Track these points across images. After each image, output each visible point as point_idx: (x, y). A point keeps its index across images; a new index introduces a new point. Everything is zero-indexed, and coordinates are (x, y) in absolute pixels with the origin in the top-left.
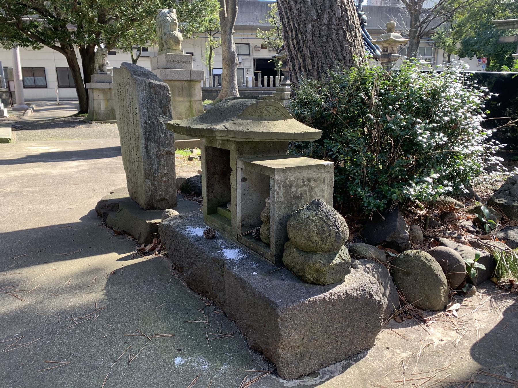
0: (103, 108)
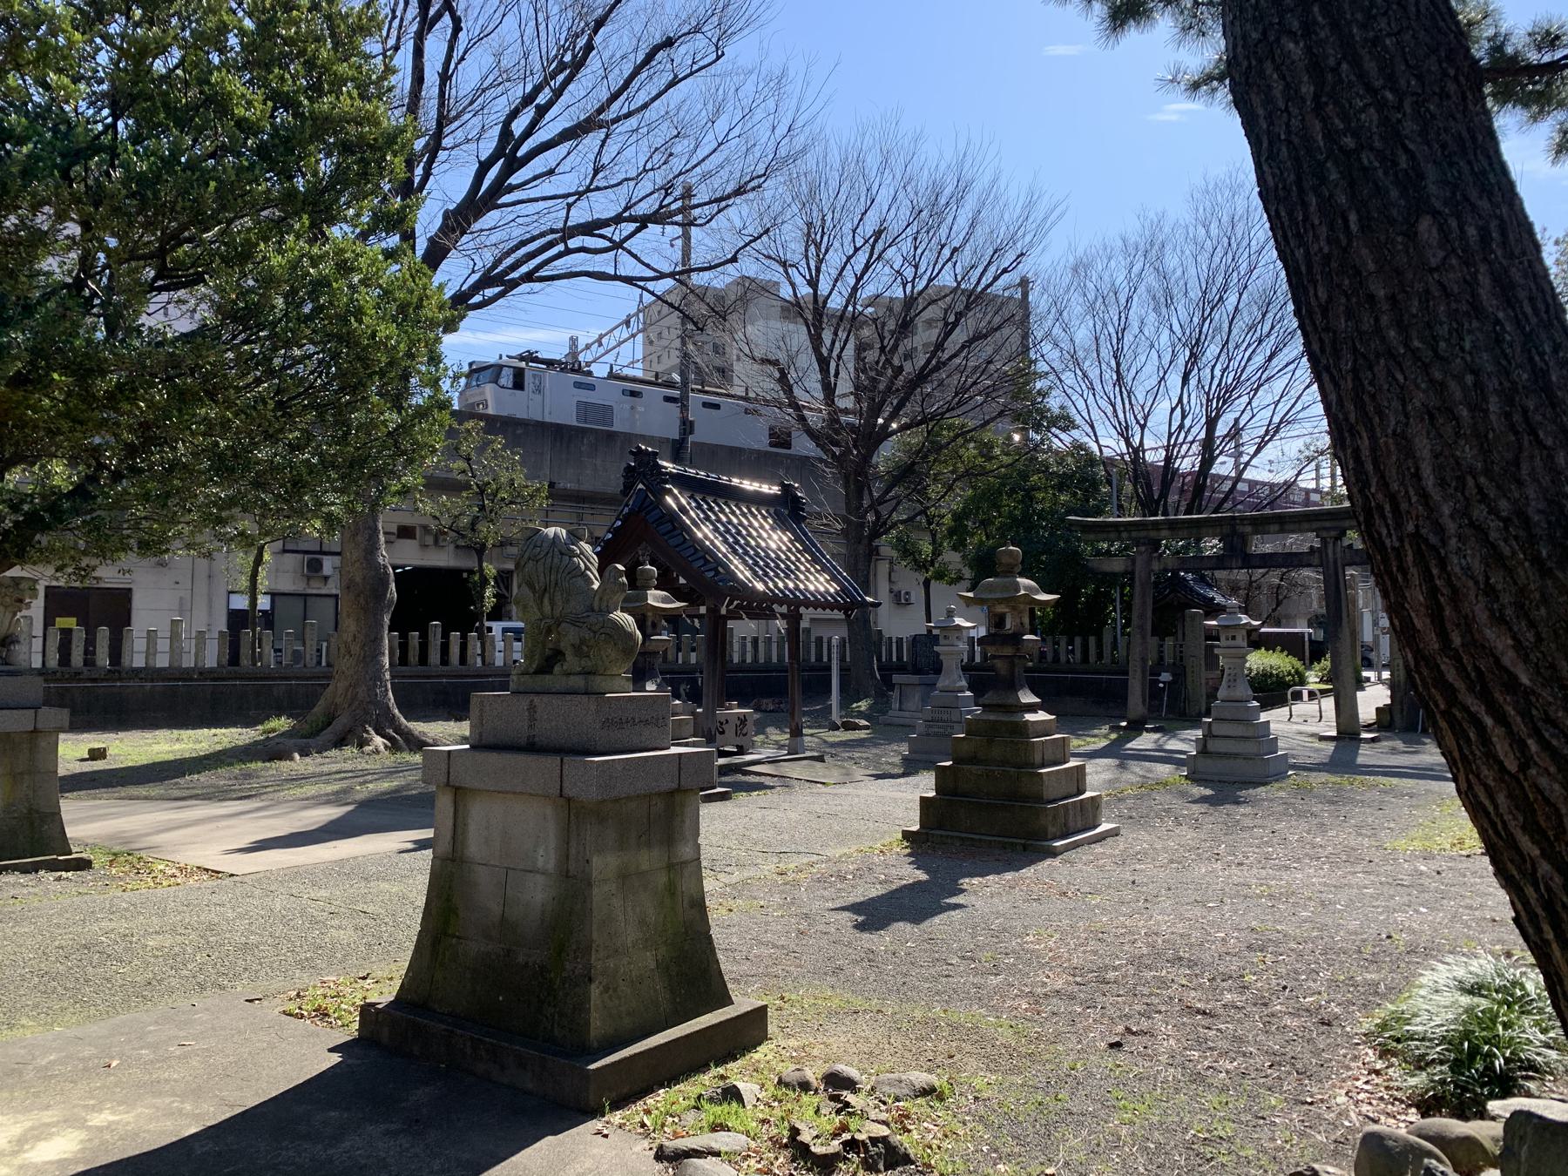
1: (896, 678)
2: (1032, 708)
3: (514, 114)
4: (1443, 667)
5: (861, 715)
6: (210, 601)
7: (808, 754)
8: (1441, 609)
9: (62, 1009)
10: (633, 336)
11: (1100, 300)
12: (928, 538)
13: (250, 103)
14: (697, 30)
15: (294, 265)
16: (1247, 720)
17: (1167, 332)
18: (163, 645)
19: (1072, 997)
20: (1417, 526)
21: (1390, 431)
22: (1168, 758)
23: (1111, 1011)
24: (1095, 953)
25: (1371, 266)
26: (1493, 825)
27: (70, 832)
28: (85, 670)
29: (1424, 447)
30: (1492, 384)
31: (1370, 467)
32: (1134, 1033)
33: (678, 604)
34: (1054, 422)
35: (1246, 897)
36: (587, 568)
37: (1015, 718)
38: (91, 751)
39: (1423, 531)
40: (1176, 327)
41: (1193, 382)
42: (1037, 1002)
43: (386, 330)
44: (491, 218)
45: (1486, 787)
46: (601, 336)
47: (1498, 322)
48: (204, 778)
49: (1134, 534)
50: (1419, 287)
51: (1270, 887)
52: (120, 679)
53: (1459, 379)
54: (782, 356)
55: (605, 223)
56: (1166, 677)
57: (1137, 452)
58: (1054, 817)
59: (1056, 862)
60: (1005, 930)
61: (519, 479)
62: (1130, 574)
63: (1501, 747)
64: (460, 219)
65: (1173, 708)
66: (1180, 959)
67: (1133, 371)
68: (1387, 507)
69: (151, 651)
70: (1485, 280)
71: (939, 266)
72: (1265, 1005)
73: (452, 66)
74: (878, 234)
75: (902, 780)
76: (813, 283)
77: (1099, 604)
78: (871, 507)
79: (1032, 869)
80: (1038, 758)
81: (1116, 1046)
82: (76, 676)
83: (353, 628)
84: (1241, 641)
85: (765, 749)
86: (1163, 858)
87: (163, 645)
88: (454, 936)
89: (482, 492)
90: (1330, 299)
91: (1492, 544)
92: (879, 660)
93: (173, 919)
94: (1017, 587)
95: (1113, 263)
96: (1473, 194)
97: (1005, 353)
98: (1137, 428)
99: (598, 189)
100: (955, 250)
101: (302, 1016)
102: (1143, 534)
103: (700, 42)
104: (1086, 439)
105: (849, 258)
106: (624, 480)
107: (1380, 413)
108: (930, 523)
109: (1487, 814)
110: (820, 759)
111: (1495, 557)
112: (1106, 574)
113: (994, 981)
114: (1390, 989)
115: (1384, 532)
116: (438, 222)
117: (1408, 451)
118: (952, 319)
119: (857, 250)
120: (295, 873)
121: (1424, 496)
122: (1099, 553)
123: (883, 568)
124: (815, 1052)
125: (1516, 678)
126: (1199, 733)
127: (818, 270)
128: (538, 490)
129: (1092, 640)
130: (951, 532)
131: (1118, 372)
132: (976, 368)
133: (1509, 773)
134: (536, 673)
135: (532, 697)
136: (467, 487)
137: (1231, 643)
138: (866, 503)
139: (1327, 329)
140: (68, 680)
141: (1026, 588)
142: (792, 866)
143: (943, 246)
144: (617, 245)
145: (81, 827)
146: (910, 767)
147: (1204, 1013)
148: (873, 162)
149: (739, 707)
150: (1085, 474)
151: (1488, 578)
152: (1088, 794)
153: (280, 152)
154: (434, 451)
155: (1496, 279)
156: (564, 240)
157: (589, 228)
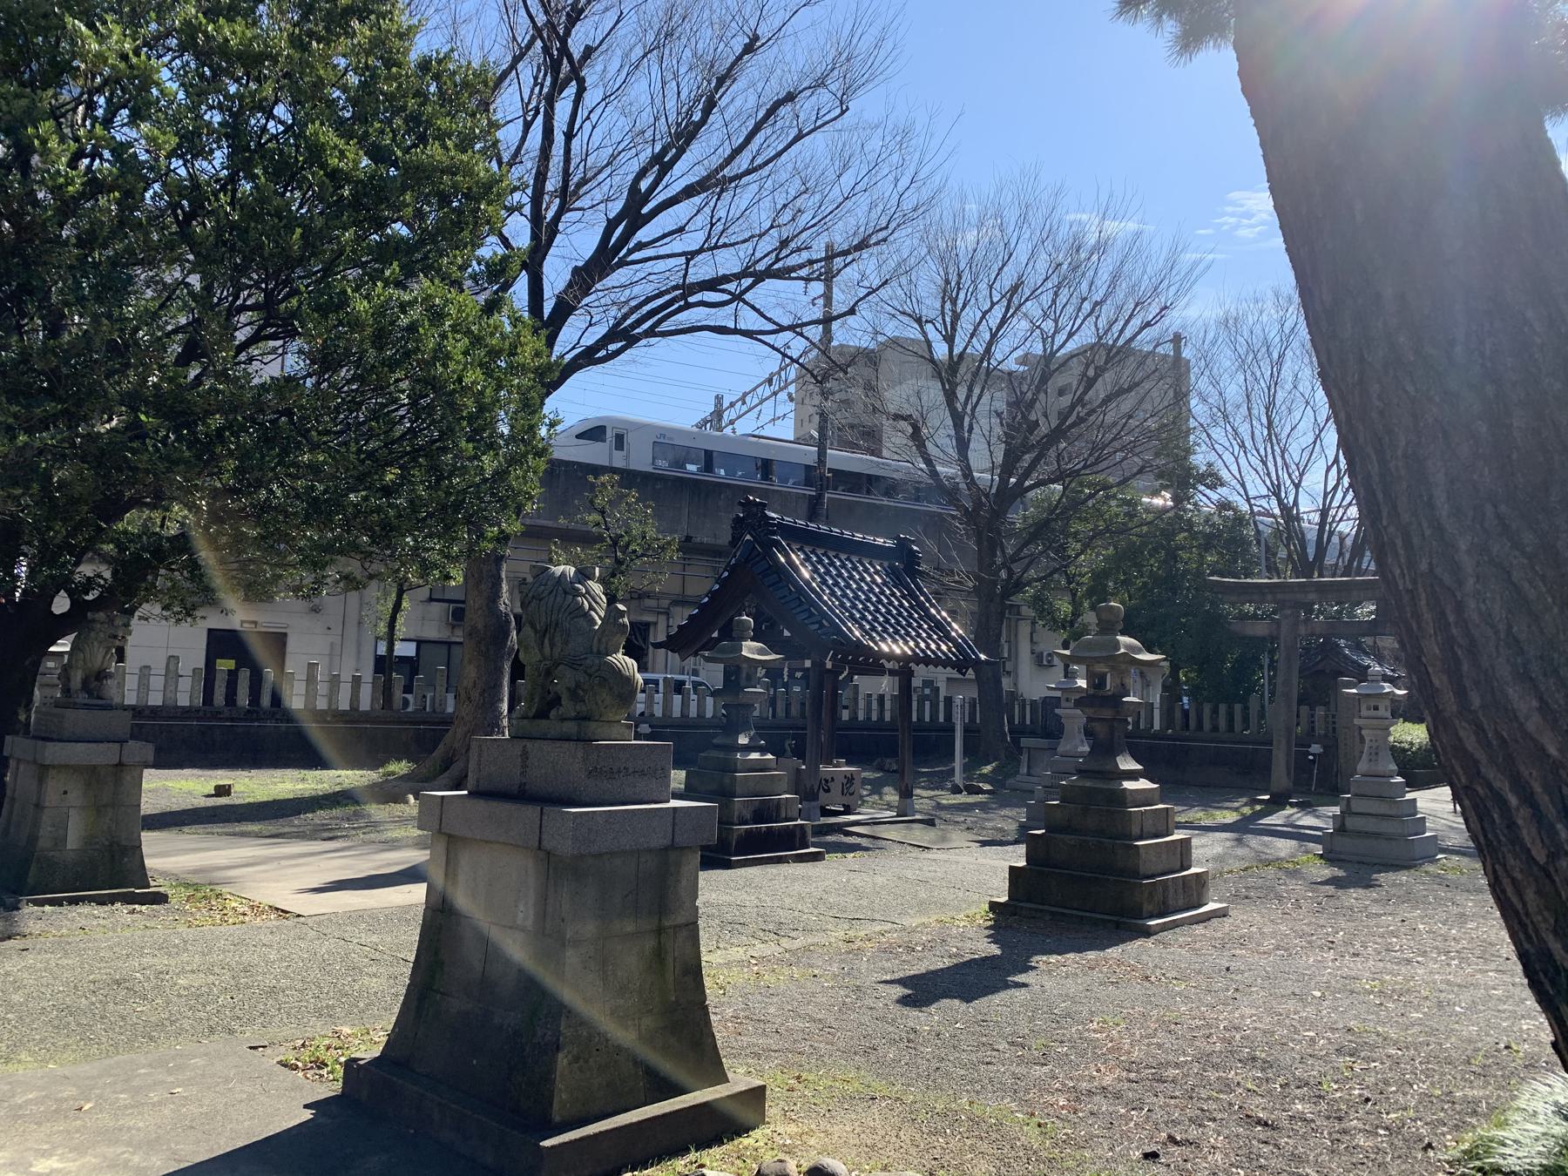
0: (73, 841)
1: (1025, 742)
2: (1132, 775)
3: (642, 174)
4: (1462, 733)
5: (984, 778)
6: (359, 644)
7: (918, 817)
9: (66, 1046)
10: (775, 394)
12: (1068, 598)
13: (342, 152)
14: (820, 83)
15: (380, 311)
16: (1388, 796)
18: (157, 682)
19: (1118, 1096)
20: (1430, 564)
21: (1399, 453)
22: (1298, 835)
23: (1158, 1115)
24: (1159, 1046)
27: (148, 862)
28: (226, 710)
31: (1380, 496)
32: (1176, 1143)
33: (773, 657)
34: (1201, 478)
35: (1352, 992)
36: (591, 608)
37: (1112, 786)
38: (218, 788)
39: (1438, 571)
42: (1078, 1099)
43: (473, 376)
44: (620, 276)
46: (745, 394)
48: (321, 816)
51: (1382, 982)
52: (258, 720)
54: (916, 415)
55: (726, 279)
56: (1316, 748)
57: (1290, 514)
58: (1151, 894)
59: (1149, 943)
60: (1068, 1015)
61: (651, 533)
62: (1273, 638)
63: (1528, 834)
64: (587, 276)
65: (1318, 779)
66: (1254, 1059)
68: (1399, 542)
69: (144, 684)
71: (1079, 321)
72: (1340, 1119)
73: (577, 127)
74: (1014, 289)
75: (1010, 848)
76: (949, 339)
78: (1004, 565)
79: (1119, 949)
80: (1136, 830)
81: (1152, 1156)
82: (216, 715)
83: (473, 675)
84: (1384, 712)
85: (873, 809)
86: (1269, 944)
87: (157, 682)
88: (438, 991)
89: (615, 543)
91: (1514, 585)
92: (1011, 721)
93: (214, 957)
94: (1117, 645)
95: (1265, 318)
97: (1147, 406)
99: (725, 245)
100: (1096, 304)
101: (297, 1067)
103: (824, 97)
105: (985, 313)
106: (734, 533)
108: (1069, 583)
109: (1517, 913)
110: (930, 823)
112: (1252, 638)
113: (1039, 1071)
114: (1491, 1108)
115: (1398, 572)
116: (567, 276)
118: (1091, 373)
119: (993, 304)
120: (356, 917)
122: (1243, 617)
123: (1024, 629)
124: (812, 1142)
125: (1543, 750)
126: (1337, 810)
127: (954, 329)
128: (669, 543)
129: (1238, 707)
130: (1090, 593)
132: (1115, 424)
133: (1536, 863)
134: (535, 717)
135: (525, 742)
136: (601, 539)
137: (1373, 713)
138: (999, 560)
140: (209, 719)
141: (1128, 647)
142: (862, 934)
143: (1084, 300)
144: (738, 297)
145: (173, 859)
147: (1266, 1124)
148: (1011, 216)
149: (848, 764)
150: (1231, 534)
151: (1510, 627)
152: (1193, 870)
153: (370, 202)
154: (531, 498)
156: (684, 297)
157: (712, 284)
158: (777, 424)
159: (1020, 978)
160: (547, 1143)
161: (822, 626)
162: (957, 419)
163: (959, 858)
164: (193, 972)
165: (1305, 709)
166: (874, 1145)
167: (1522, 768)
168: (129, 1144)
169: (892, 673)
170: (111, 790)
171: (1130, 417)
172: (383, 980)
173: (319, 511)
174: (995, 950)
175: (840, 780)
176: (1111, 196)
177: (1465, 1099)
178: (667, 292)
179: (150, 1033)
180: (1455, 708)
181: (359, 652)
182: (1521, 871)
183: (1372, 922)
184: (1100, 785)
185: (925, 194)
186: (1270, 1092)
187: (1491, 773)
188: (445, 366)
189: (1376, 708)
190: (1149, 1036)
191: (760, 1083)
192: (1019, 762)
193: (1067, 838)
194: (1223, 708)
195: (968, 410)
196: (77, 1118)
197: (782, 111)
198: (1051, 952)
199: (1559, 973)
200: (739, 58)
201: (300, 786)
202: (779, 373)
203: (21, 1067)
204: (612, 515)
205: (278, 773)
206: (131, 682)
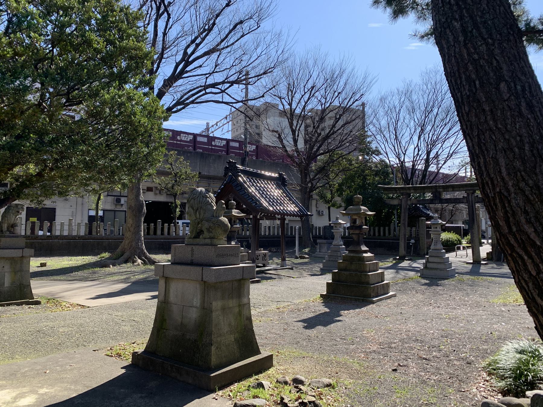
1: (318, 241)
2: (366, 252)
3: (188, 46)
5: (306, 254)
7: (287, 267)
8: (509, 218)
11: (390, 110)
12: (330, 192)
13: (98, 43)
14: (251, 18)
15: (113, 98)
16: (441, 256)
17: (413, 122)
18: (66, 227)
19: (379, 353)
20: (500, 189)
22: (413, 270)
23: (393, 358)
24: (387, 337)
25: (484, 99)
26: (527, 294)
27: (34, 291)
29: (502, 162)
30: (526, 140)
32: (401, 366)
33: (243, 215)
34: (373, 152)
36: (212, 202)
37: (360, 255)
38: (41, 264)
40: (416, 120)
41: (422, 139)
42: (367, 355)
43: (144, 120)
45: (525, 281)
46: (217, 122)
47: (528, 119)
48: (80, 273)
49: (402, 191)
50: (501, 106)
51: (449, 315)
52: (52, 239)
53: (515, 138)
56: (413, 241)
57: (402, 163)
59: (374, 306)
60: (356, 329)
61: (189, 171)
62: (400, 205)
63: (530, 267)
64: (169, 82)
65: (415, 252)
66: (417, 340)
67: (401, 135)
68: (490, 182)
70: (523, 104)
72: (448, 357)
74: (313, 88)
76: (290, 104)
77: (389, 215)
78: (310, 181)
80: (368, 269)
81: (395, 370)
84: (439, 229)
85: (273, 265)
86: (412, 304)
87: (66, 227)
89: (176, 175)
90: (469, 111)
91: (526, 196)
92: (312, 234)
93: (68, 322)
94: (360, 209)
96: (519, 75)
97: (356, 128)
98: (402, 155)
99: (216, 72)
100: (339, 93)
101: (112, 356)
102: (404, 191)
103: (252, 22)
104: (385, 158)
107: (487, 150)
109: (526, 290)
110: (292, 269)
111: (527, 200)
112: (391, 205)
113: (352, 347)
114: (492, 352)
115: (489, 191)
117: (497, 163)
120: (110, 307)
121: (503, 179)
122: (389, 198)
123: (314, 202)
124: (290, 371)
125: (535, 242)
126: (424, 261)
128: (195, 175)
129: (387, 228)
131: (396, 135)
135: (192, 246)
136: (171, 174)
137: (435, 229)
138: (308, 180)
139: (469, 121)
141: (364, 210)
142: (282, 306)
144: (223, 91)
145: (37, 290)
146: (323, 272)
147: (426, 359)
148: (311, 63)
150: (384, 170)
151: (525, 208)
152: (385, 282)
154: (160, 161)
155: (527, 104)
156: (205, 89)
157: (213, 86)
158: (225, 132)
159: (338, 319)
160: (212, 375)
161: (256, 204)
162: (293, 132)
163: (305, 280)
164: (63, 327)
165: (409, 228)
166: (309, 372)
167: (529, 248)
168: (68, 383)
169: (279, 219)
170: (19, 265)
171: (351, 132)
172: (129, 327)
173: (89, 166)
174: (327, 310)
175: (262, 255)
176: (344, 56)
177: (483, 349)
178: (197, 88)
179: (59, 347)
180: (507, 231)
181: (82, 214)
182: (528, 278)
183: (440, 297)
184: (357, 255)
185: (286, 56)
186: (425, 349)
187: (518, 250)
188: (135, 117)
189: (436, 228)
190: (383, 335)
191: (271, 354)
192: (316, 249)
193: (345, 272)
194: (382, 229)
195: (297, 129)
196: (46, 376)
197: (238, 27)
198: (345, 310)
199: (539, 307)
200: (224, 8)
201: (70, 262)
202: (229, 115)
203: (18, 360)
204: (175, 165)
205: (61, 258)
206: (58, 227)
